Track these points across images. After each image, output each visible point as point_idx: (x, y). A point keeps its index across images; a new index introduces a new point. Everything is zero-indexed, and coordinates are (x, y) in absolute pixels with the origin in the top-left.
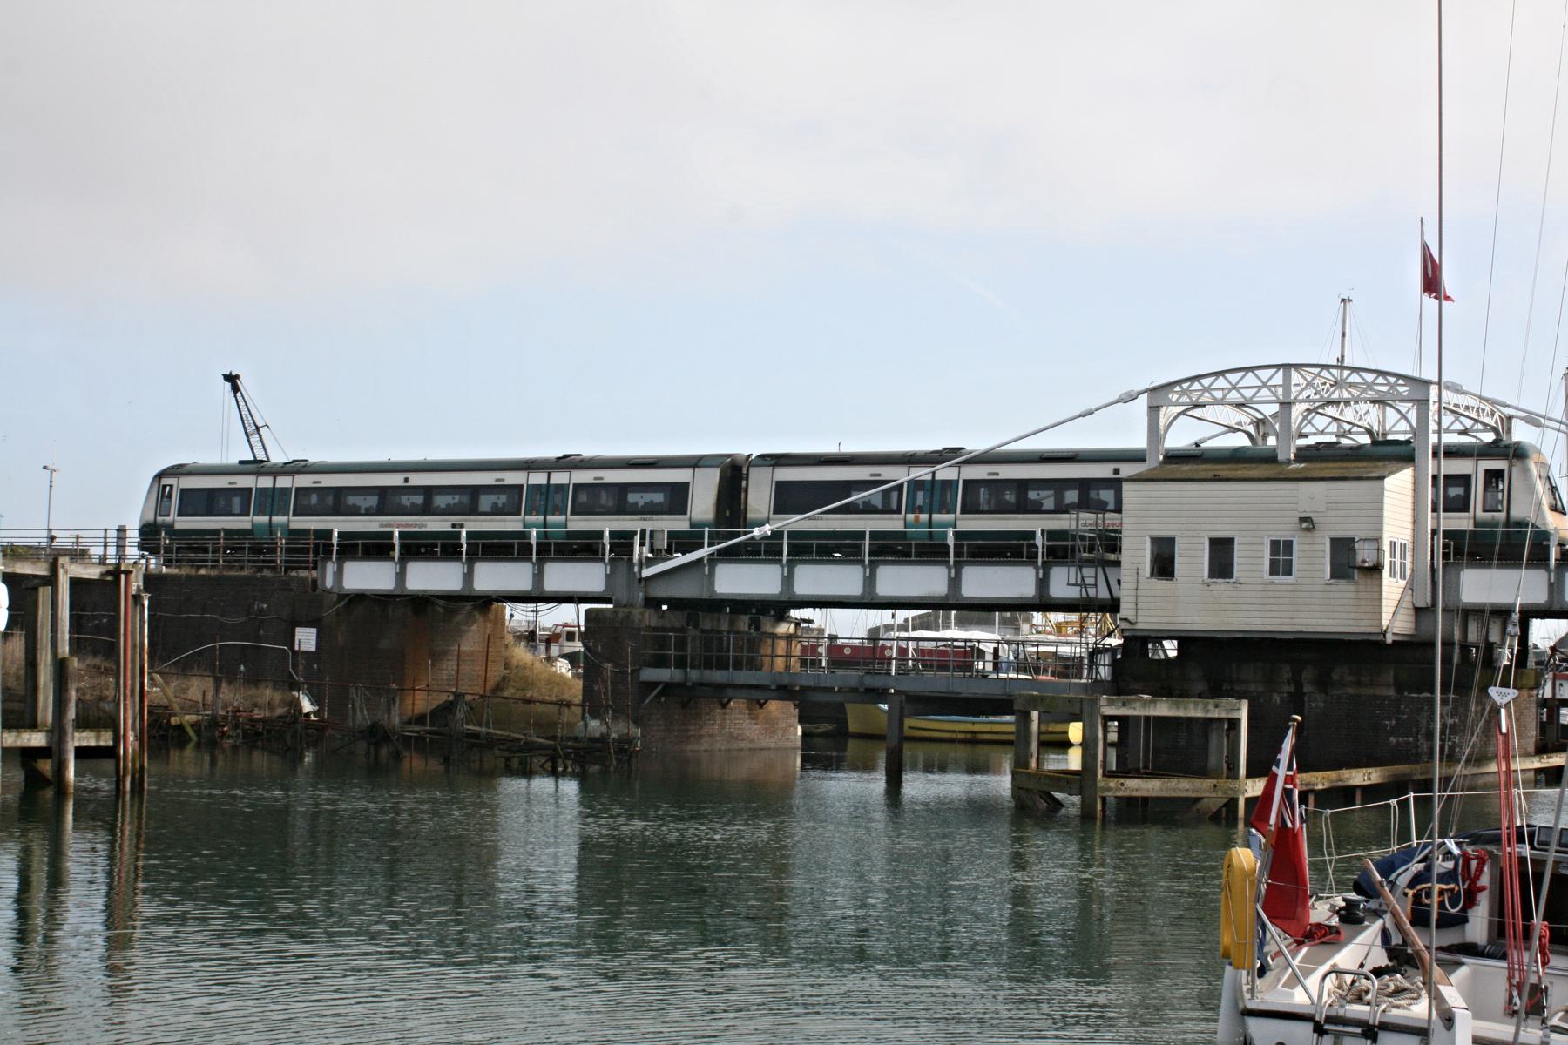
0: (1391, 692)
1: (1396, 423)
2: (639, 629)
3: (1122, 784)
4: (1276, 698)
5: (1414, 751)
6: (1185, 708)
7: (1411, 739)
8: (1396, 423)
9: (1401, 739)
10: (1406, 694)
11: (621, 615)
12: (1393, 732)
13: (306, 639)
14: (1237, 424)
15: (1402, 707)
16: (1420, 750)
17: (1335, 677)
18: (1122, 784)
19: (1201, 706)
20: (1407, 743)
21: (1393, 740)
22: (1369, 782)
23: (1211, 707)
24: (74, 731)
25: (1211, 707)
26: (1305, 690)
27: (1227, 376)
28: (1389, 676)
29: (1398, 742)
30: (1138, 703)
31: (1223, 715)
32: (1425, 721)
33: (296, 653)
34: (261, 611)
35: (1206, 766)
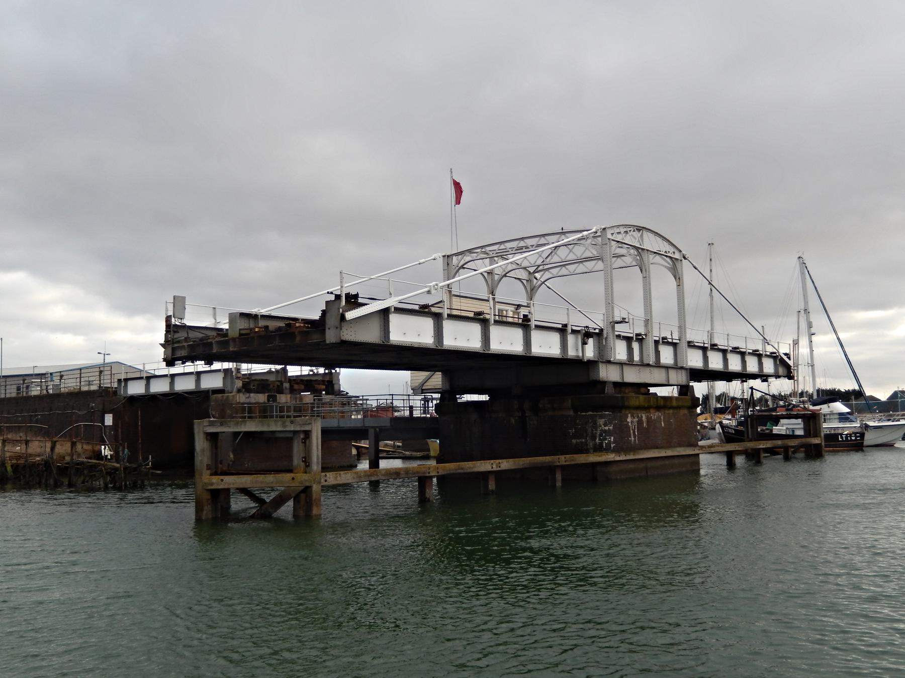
0: (571, 413)
1: (584, 252)
2: (232, 404)
3: (222, 480)
4: (513, 420)
5: (585, 447)
6: (269, 425)
7: (584, 440)
8: (584, 252)
9: (578, 441)
10: (579, 413)
11: (225, 398)
12: (575, 436)
13: (109, 420)
14: (786, 354)
15: (578, 421)
16: (588, 447)
17: (541, 406)
18: (222, 480)
19: (280, 423)
20: (582, 443)
21: (574, 441)
22: (499, 469)
23: (288, 423)
24: (821, 444)
25: (288, 423)
26: (527, 415)
27: (567, 267)
28: (569, 403)
29: (577, 442)
30: (232, 423)
31: (298, 428)
32: (590, 429)
33: (106, 427)
34: (92, 408)
35: (292, 465)
